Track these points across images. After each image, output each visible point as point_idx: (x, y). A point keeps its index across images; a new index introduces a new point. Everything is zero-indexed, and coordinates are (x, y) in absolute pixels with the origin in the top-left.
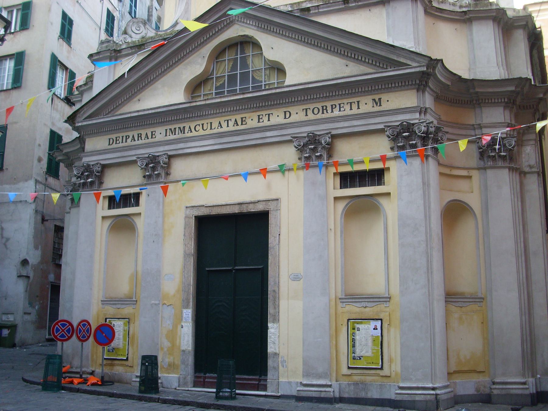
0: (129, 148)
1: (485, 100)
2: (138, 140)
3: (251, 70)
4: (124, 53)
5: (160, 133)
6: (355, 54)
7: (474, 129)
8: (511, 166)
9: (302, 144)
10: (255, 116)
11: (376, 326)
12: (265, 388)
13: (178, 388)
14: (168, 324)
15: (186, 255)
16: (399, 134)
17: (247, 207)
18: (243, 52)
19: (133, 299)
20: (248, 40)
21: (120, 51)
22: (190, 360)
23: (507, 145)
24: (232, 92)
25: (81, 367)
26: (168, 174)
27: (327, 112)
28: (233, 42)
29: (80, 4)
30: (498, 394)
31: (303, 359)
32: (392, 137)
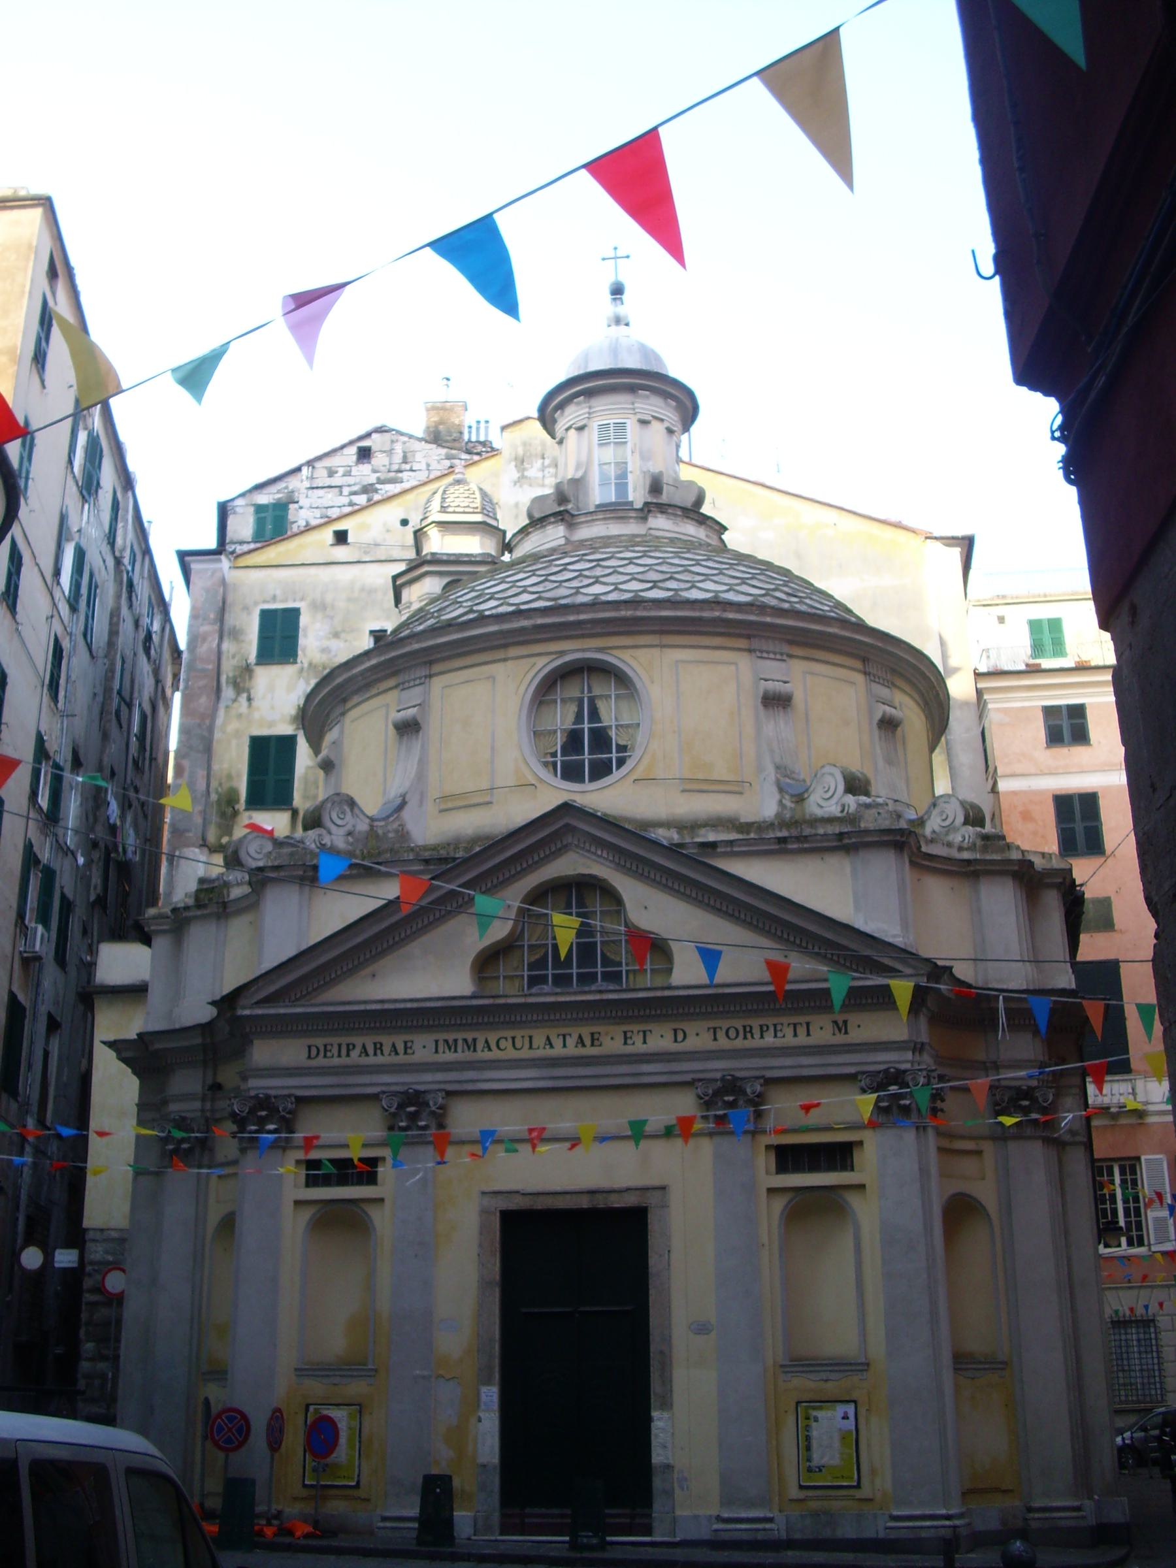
2: (375, 1054)
5: (423, 1047)
9: (710, 1092)
10: (618, 1031)
11: (846, 1413)
12: (648, 1531)
13: (473, 1538)
15: (484, 1284)
22: (495, 1481)
23: (1040, 1100)
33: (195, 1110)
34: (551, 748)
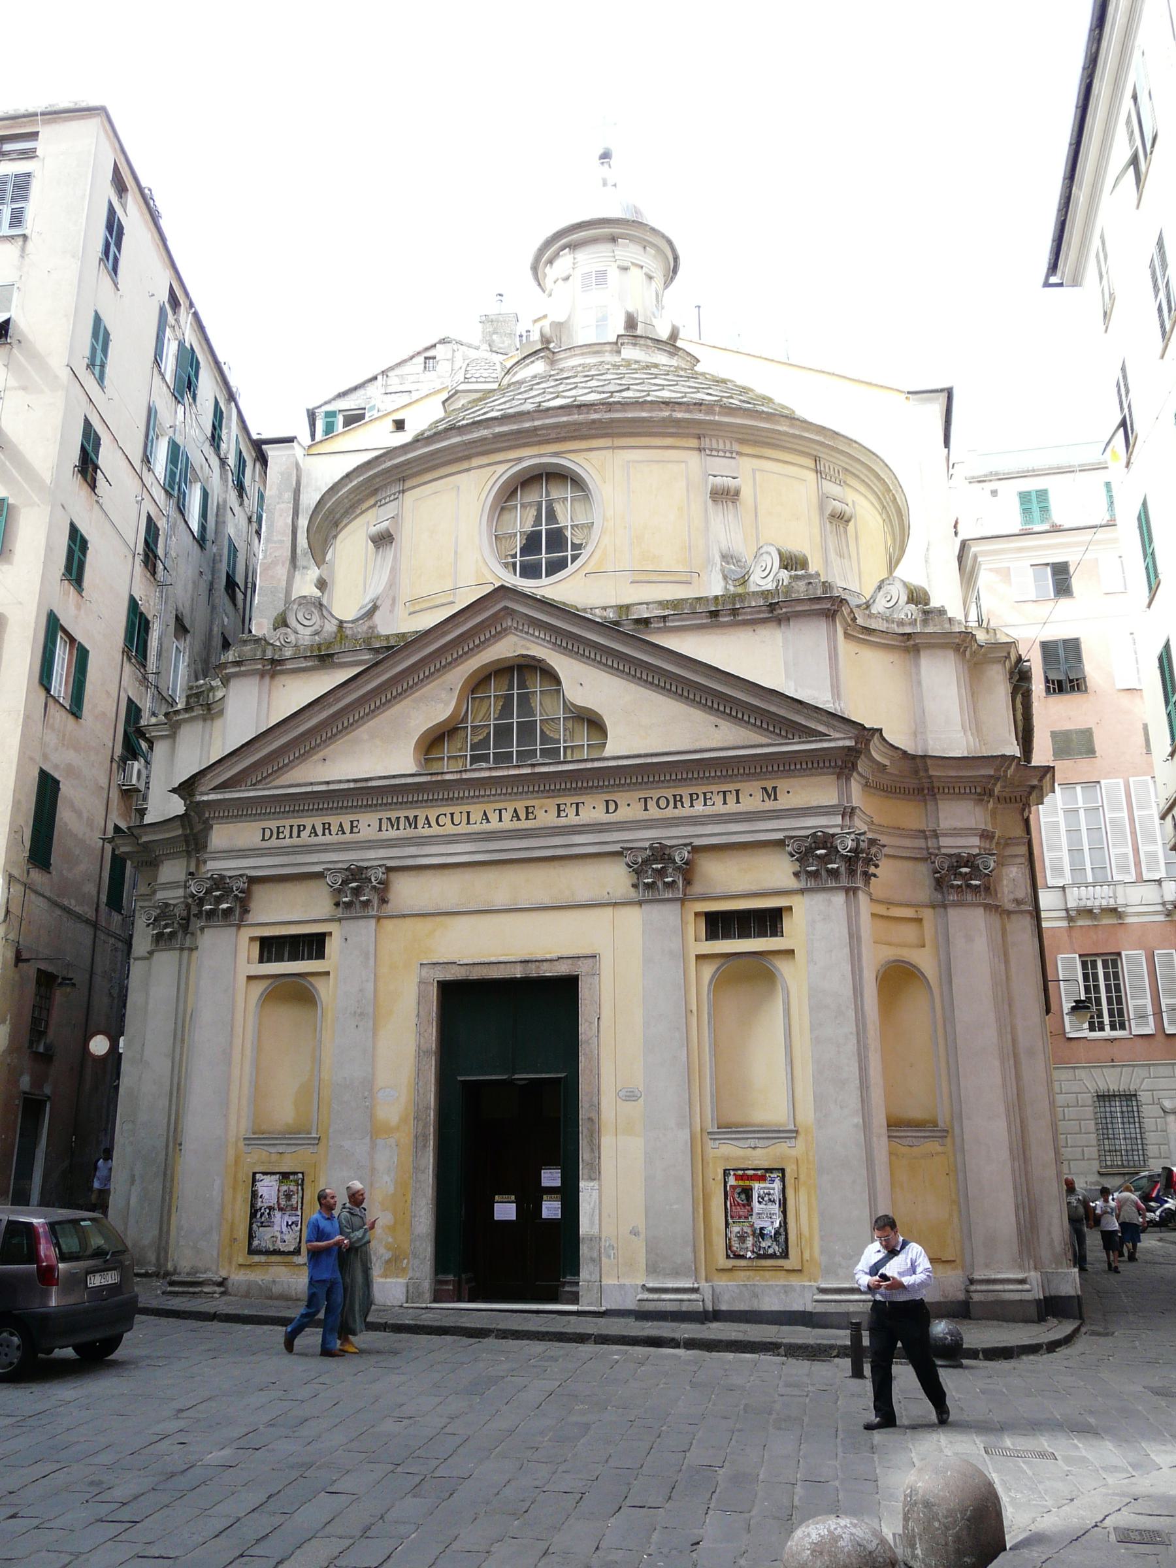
0: (305, 849)
2: (324, 834)
4: (289, 666)
5: (368, 825)
9: (640, 860)
10: (551, 804)
12: (574, 1298)
15: (420, 1052)
16: (810, 851)
20: (533, 663)
24: (503, 758)
26: (384, 901)
27: (683, 806)
28: (506, 665)
30: (981, 1302)
32: (797, 856)
33: (179, 897)
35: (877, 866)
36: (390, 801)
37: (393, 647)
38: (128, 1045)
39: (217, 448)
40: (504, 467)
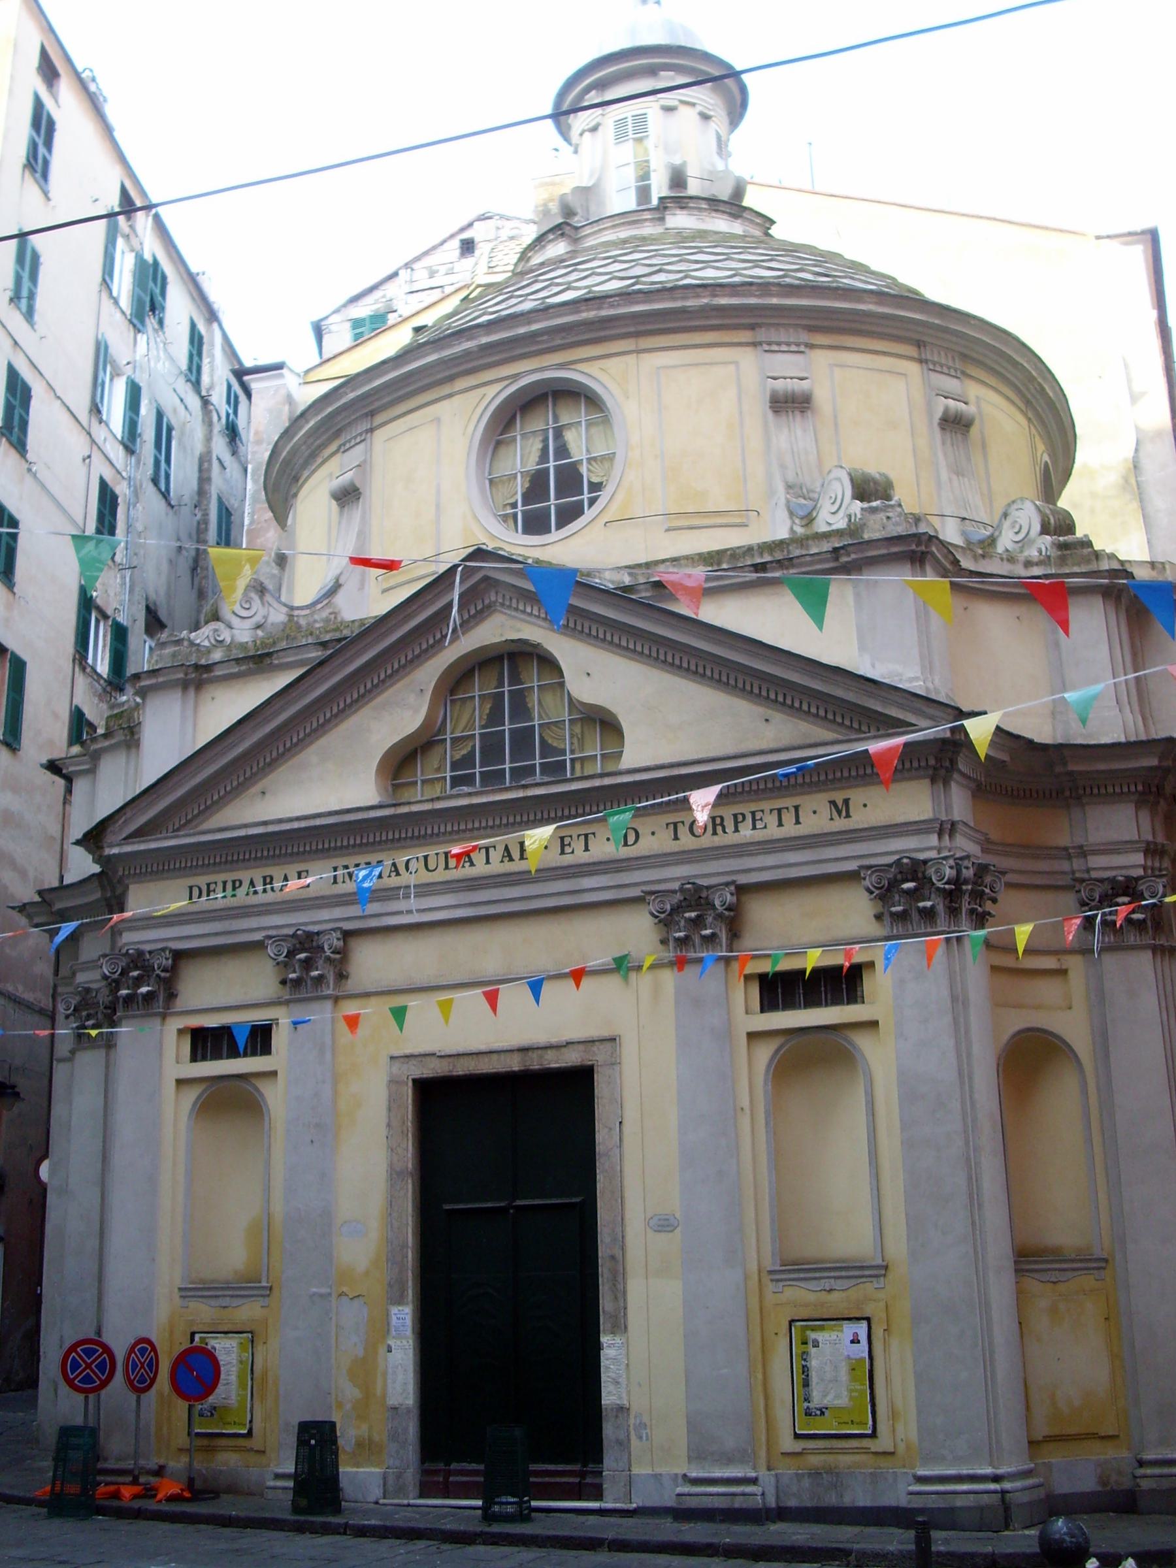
1: (1091, 788)
3: (536, 723)
4: (218, 672)
6: (785, 695)
7: (1069, 857)
8: (1158, 943)
9: (668, 907)
12: (599, 1496)
13: (381, 1501)
14: (352, 1345)
15: (394, 1174)
16: (893, 884)
17: (541, 1057)
18: (515, 679)
19: (260, 1282)
20: (530, 649)
21: (208, 668)
22: (412, 1429)
24: (493, 779)
25: (136, 1456)
26: (342, 976)
27: (724, 832)
29: (35, 475)
31: (687, 1416)
32: (877, 892)
34: (512, 497)
35: (994, 901)
36: (345, 843)
37: (345, 638)
38: (52, 1172)
39: (196, 384)
40: (497, 387)
